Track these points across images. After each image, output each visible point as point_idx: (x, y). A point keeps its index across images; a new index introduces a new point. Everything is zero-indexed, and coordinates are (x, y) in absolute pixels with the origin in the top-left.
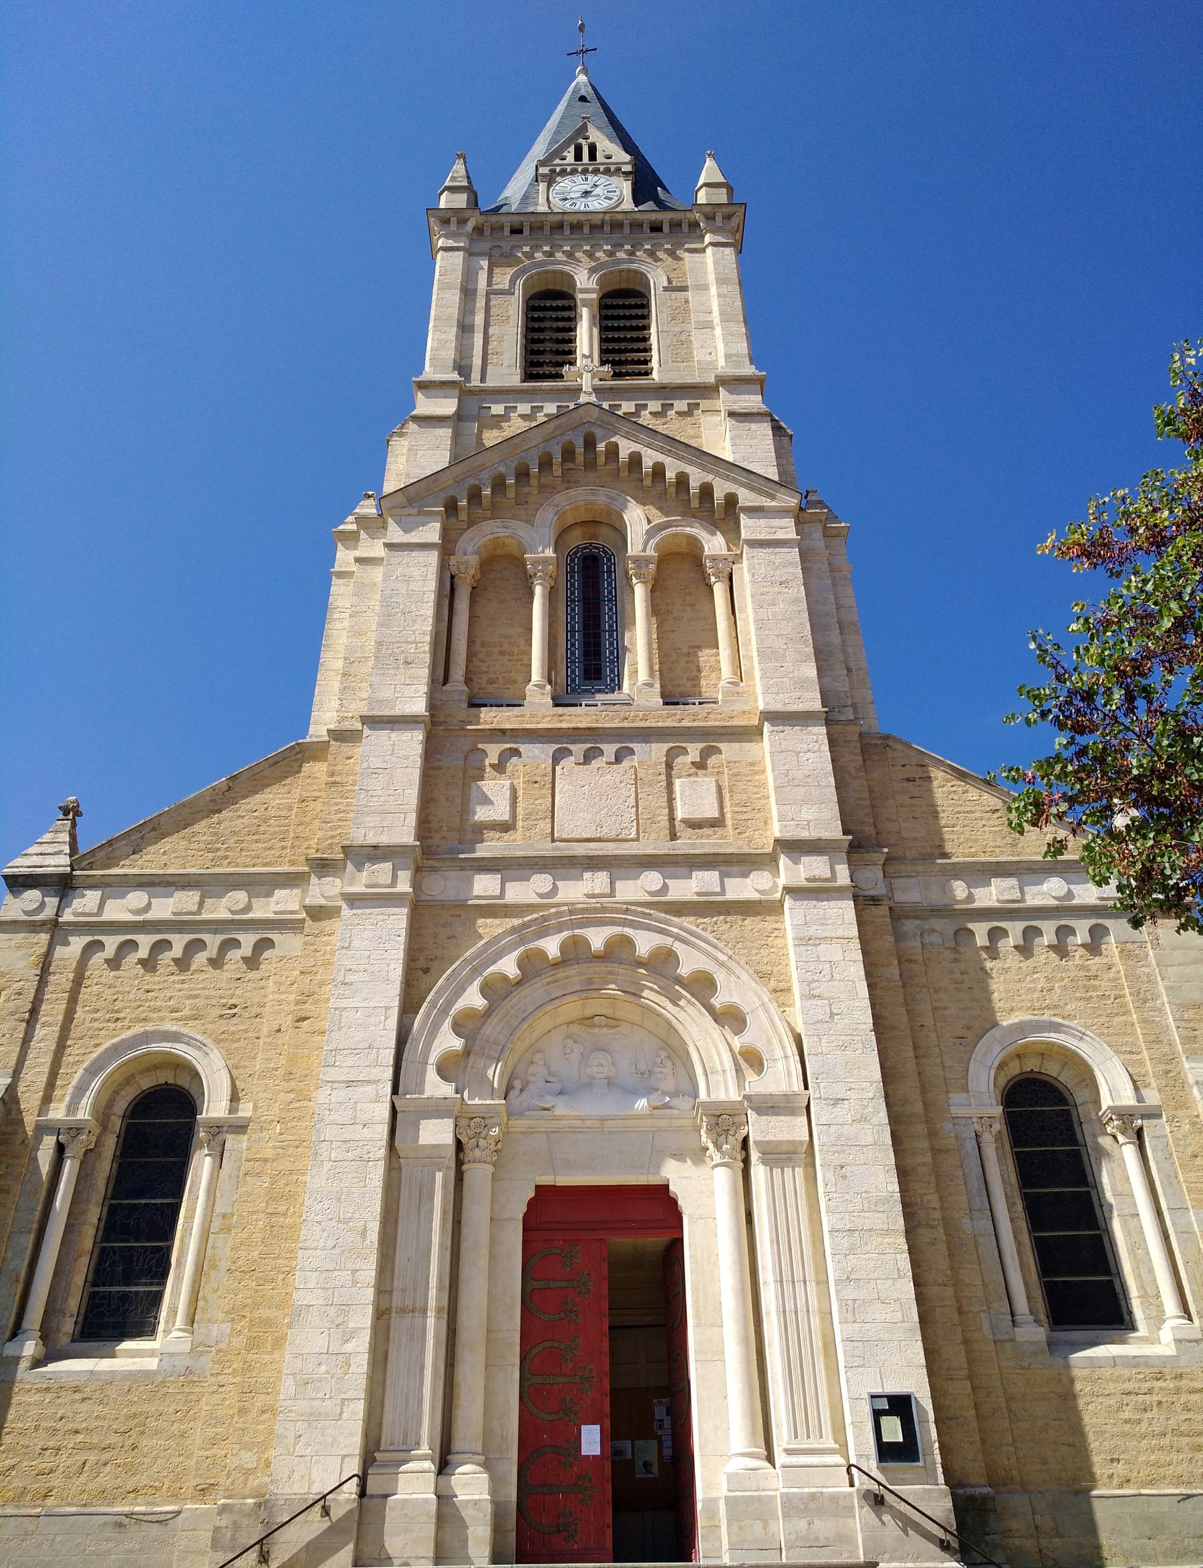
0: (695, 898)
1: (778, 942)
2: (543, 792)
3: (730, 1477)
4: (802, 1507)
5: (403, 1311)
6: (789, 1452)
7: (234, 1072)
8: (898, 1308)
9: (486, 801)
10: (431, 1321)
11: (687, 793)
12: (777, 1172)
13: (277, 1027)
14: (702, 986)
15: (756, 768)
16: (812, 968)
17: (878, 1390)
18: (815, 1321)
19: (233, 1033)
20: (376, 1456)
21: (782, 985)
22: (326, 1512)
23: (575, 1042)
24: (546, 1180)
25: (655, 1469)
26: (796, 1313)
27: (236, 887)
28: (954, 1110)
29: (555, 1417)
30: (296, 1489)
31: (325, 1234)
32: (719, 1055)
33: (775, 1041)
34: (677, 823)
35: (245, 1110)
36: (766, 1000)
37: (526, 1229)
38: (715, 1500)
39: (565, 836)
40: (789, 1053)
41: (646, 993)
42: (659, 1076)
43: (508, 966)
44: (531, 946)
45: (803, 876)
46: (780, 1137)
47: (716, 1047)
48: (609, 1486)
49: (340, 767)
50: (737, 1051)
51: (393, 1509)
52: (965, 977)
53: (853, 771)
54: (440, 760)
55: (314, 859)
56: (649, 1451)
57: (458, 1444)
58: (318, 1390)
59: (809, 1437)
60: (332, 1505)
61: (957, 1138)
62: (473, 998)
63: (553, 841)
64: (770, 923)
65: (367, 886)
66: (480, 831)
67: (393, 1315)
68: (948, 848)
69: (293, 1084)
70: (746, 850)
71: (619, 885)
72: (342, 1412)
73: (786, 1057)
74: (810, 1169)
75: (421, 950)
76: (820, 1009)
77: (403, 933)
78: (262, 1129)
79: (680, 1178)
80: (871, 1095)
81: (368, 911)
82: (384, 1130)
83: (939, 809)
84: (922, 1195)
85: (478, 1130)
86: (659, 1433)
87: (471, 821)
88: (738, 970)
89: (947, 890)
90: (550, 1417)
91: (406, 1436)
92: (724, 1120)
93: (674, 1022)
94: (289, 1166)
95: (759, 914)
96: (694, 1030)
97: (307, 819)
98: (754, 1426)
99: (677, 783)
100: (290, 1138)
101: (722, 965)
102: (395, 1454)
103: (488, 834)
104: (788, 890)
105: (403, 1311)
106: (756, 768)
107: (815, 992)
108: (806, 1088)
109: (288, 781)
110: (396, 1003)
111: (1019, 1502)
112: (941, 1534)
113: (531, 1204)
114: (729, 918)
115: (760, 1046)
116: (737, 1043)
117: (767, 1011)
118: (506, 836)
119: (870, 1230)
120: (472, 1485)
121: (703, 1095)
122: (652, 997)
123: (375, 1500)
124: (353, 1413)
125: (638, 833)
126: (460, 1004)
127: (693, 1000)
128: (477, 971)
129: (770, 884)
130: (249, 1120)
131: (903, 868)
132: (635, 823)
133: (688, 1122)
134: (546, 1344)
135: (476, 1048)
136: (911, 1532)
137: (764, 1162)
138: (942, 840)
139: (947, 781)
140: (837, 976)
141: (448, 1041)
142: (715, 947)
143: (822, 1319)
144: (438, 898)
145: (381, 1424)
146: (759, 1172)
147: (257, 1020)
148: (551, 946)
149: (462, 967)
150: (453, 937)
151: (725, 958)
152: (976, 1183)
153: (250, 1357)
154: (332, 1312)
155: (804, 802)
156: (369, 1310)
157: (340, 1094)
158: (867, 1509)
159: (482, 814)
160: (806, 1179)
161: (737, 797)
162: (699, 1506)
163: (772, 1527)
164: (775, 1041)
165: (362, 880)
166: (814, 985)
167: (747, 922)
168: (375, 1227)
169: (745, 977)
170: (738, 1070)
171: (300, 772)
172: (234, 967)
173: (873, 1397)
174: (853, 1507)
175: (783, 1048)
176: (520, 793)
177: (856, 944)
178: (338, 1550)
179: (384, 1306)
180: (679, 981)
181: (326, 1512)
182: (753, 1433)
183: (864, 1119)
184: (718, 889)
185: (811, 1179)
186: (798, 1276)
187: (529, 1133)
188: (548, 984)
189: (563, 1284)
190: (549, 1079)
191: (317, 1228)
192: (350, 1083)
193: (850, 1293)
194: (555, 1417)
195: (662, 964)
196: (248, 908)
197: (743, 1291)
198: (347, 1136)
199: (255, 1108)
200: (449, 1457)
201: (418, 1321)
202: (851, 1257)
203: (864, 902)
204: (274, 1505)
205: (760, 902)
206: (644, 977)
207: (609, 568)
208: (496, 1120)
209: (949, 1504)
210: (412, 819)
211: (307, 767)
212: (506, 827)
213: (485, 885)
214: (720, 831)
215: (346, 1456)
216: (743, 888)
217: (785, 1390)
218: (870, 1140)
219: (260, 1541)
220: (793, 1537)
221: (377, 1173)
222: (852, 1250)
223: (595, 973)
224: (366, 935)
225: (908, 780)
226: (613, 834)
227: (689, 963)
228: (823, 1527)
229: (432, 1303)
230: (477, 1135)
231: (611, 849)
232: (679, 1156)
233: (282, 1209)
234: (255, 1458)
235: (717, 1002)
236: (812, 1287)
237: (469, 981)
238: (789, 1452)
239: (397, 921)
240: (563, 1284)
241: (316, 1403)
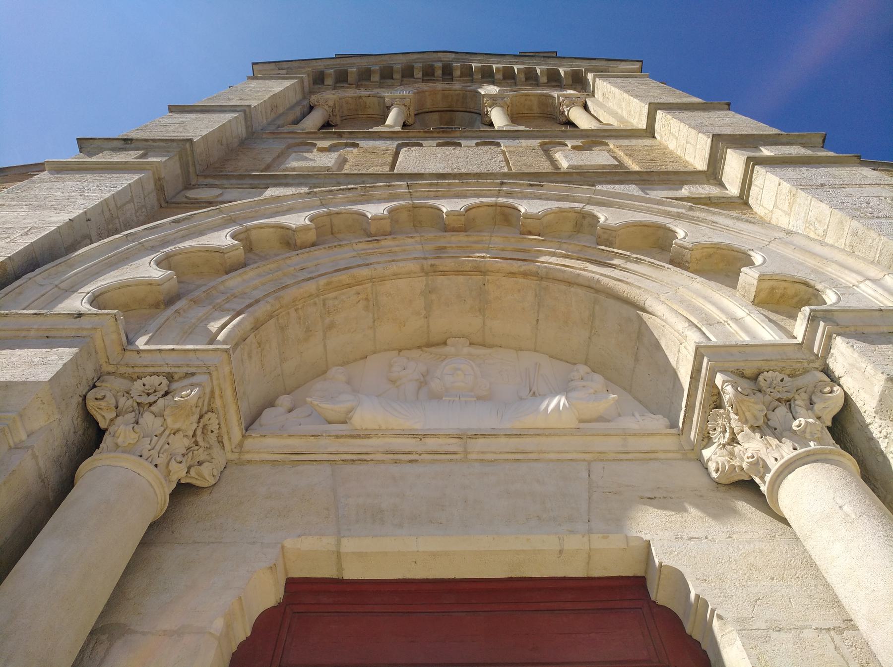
24: (318, 553)
113: (267, 623)
232: (666, 499)
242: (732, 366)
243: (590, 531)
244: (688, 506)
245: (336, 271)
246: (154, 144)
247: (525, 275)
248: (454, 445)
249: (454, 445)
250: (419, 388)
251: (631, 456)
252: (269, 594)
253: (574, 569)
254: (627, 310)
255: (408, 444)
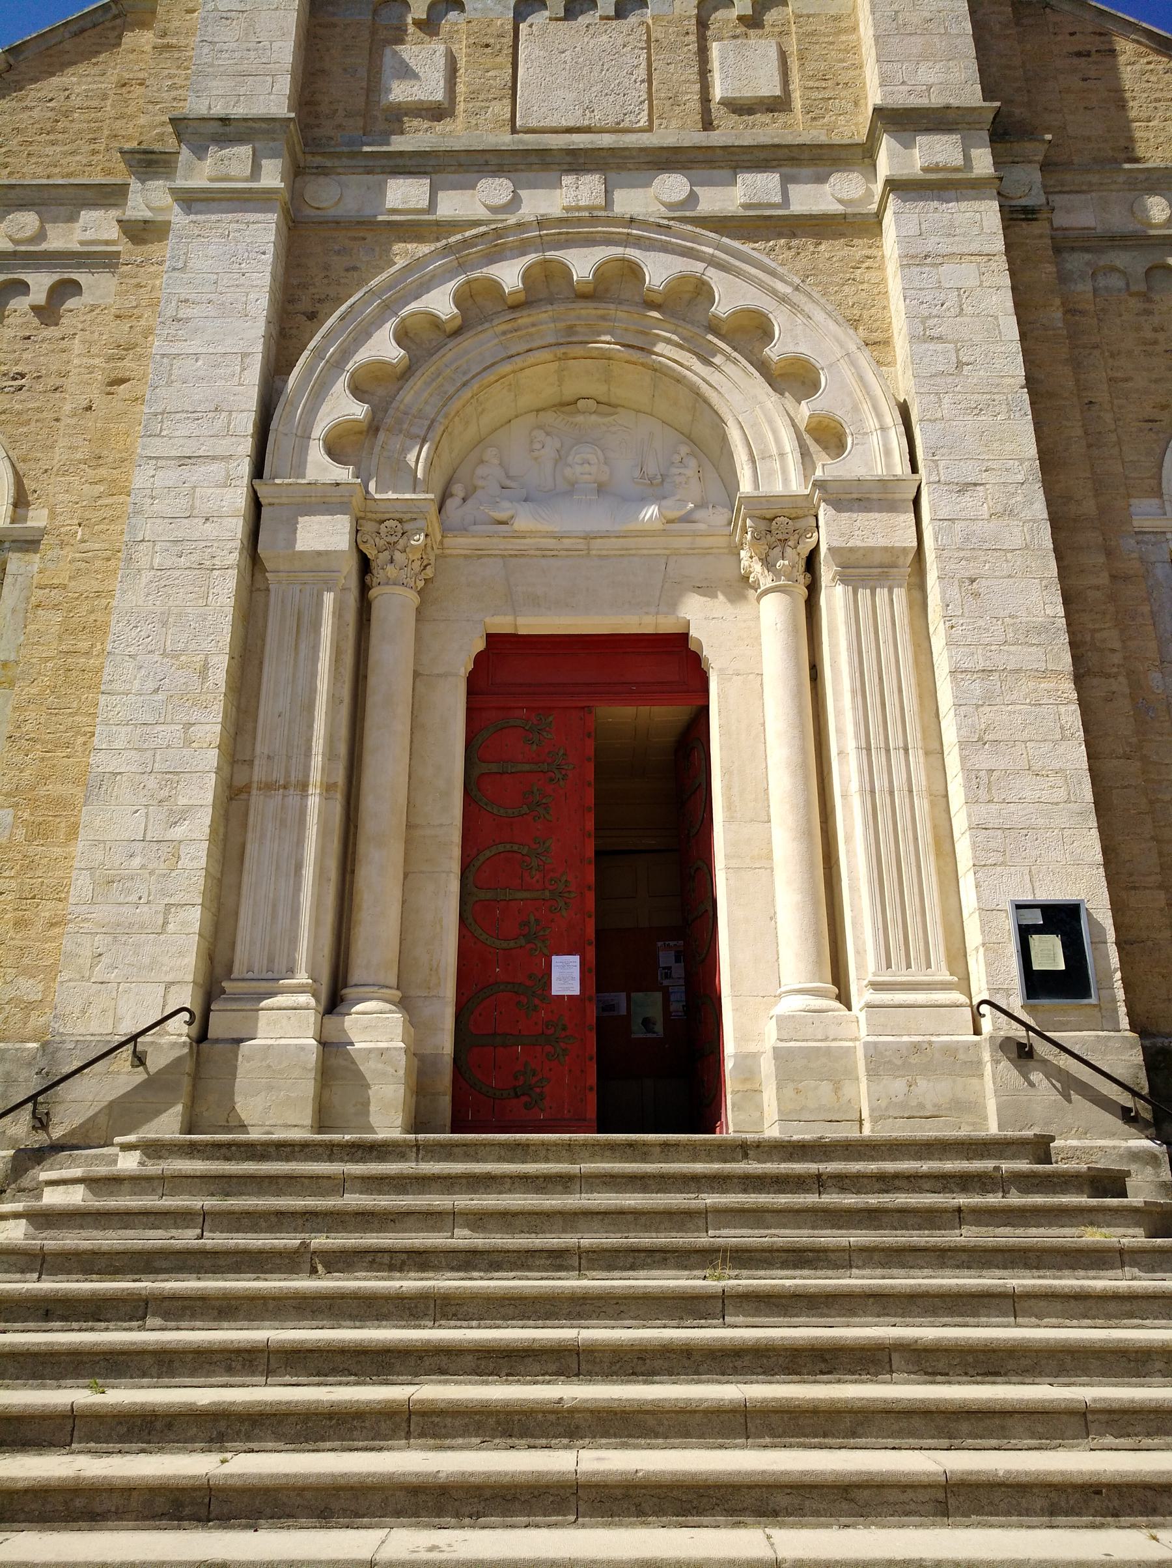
0: (741, 212)
1: (873, 276)
2: (499, 59)
3: (782, 1021)
4: (899, 1062)
5: (269, 787)
6: (877, 986)
7: (20, 466)
8: (1060, 782)
9: (407, 73)
10: (314, 801)
11: (731, 60)
12: (864, 594)
13: (85, 403)
14: (750, 333)
15: (843, 25)
16: (928, 298)
17: (1027, 897)
18: (922, 806)
19: (19, 413)
20: (222, 983)
21: (876, 336)
22: (139, 1059)
23: (548, 434)
24: (503, 624)
25: (659, 1028)
26: (892, 793)
27: (22, 206)
28: (1138, 522)
29: (512, 944)
30: (94, 1027)
31: (143, 671)
32: (775, 432)
33: (866, 408)
34: (714, 106)
35: (37, 518)
36: (852, 347)
37: (471, 692)
38: (755, 1056)
39: (533, 123)
40: (888, 420)
41: (660, 348)
42: (678, 479)
43: (441, 302)
44: (476, 274)
45: (918, 164)
46: (871, 542)
47: (770, 422)
48: (593, 1037)
49: (177, 24)
50: (802, 427)
51: (249, 1059)
52: (1161, 336)
53: (997, 28)
54: (334, 14)
55: (132, 152)
56: (651, 1005)
57: (357, 974)
58: (129, 892)
59: (909, 966)
60: (149, 1050)
61: (1141, 560)
62: (383, 347)
63: (514, 131)
64: (859, 248)
65: (211, 180)
66: (397, 117)
67: (254, 792)
68: (1141, 150)
69: (103, 472)
70: (823, 139)
71: (619, 195)
72: (165, 923)
73: (883, 429)
74: (917, 594)
75: (304, 286)
76: (940, 357)
77: (271, 247)
78: (62, 545)
79: (704, 620)
80: (1020, 478)
81: (214, 217)
82: (237, 527)
83: (1128, 95)
84: (1095, 631)
85: (393, 539)
86: (666, 983)
87: (383, 102)
88: (808, 307)
89: (1134, 209)
90: (504, 945)
91: (271, 960)
92: (777, 523)
93: (704, 387)
94: (96, 585)
95: (842, 235)
96: (735, 398)
97: (129, 111)
98: (819, 954)
99: (715, 50)
100: (97, 546)
101: (783, 300)
102: (254, 984)
103: (411, 123)
104: (894, 185)
105: (269, 787)
106: (843, 25)
107: (935, 333)
108: (915, 469)
109: (102, 57)
110: (258, 348)
112: (1126, 1100)
113: (480, 659)
114: (794, 242)
115: (841, 414)
116: (804, 411)
117: (853, 363)
118: (439, 127)
119: (1017, 671)
120: (376, 1029)
121: (746, 487)
122: (667, 352)
123: (219, 1047)
124: (183, 924)
125: (650, 120)
126: (363, 355)
127: (735, 354)
128: (388, 309)
129: (861, 192)
130: (43, 531)
131: (1068, 177)
132: (646, 106)
133: (722, 541)
134: (501, 848)
135: (389, 421)
136: (1075, 1097)
137: (844, 579)
138: (1131, 139)
139: (1140, 55)
140: (968, 310)
141: (343, 407)
142: (773, 273)
143: (933, 805)
144: (332, 212)
145: (233, 945)
146: (834, 598)
147: (57, 395)
148: (509, 275)
149: (365, 302)
150: (355, 269)
151: (788, 290)
153: (31, 850)
154: (152, 782)
155: (923, 57)
156: (211, 780)
157: (170, 476)
158: (1005, 1064)
159: (400, 92)
160: (911, 606)
161: (811, 67)
162: (729, 1064)
163: (848, 1090)
164: (866, 408)
165: (200, 172)
166: (930, 322)
167: (822, 247)
168: (220, 664)
169: (819, 316)
170: (805, 454)
171: (119, 45)
172: (20, 320)
173: (1019, 907)
174: (980, 1063)
175: (879, 415)
176: (462, 63)
177: (1002, 263)
178: (158, 1113)
179: (240, 781)
180: (713, 327)
181: (139, 1059)
182: (818, 962)
183: (1008, 512)
184: (778, 199)
185: (919, 605)
186: (895, 741)
187: (478, 555)
188: (504, 333)
189: (527, 767)
190: (508, 483)
191: (130, 665)
192: (184, 460)
193: (984, 760)
194: (512, 944)
195: (687, 303)
196: (41, 236)
197: (804, 765)
198: (180, 535)
199: (53, 515)
200: (344, 992)
201: (293, 799)
202: (987, 709)
203: (1015, 216)
204: (57, 1050)
205: (845, 216)
206: (658, 323)
208: (420, 523)
209: (1137, 1057)
210: (284, 85)
211: (129, 38)
212: (438, 112)
213: (404, 194)
214: (782, 118)
215: (173, 983)
216: (814, 198)
217: (873, 904)
218: (1018, 542)
219: (33, 1098)
220: (883, 1103)
221: (225, 590)
222: (988, 699)
223: (579, 318)
224: (212, 250)
225: (1079, 54)
226: (611, 121)
227: (729, 296)
228: (931, 1090)
229: (316, 776)
230: (391, 546)
232: (706, 589)
233: (84, 645)
234: (41, 987)
235: (773, 352)
236: (917, 758)
237: (377, 322)
238: (877, 986)
239: (261, 234)
240: (527, 767)
241: (124, 909)
242: (758, 513)
243: (657, 613)
244: (719, 594)
245: (485, 369)
246: (254, 125)
247: (642, 364)
248: (581, 544)
249: (581, 544)
250: (556, 465)
251: (696, 551)
252: (480, 645)
253: (649, 630)
254: (718, 420)
255: (550, 543)
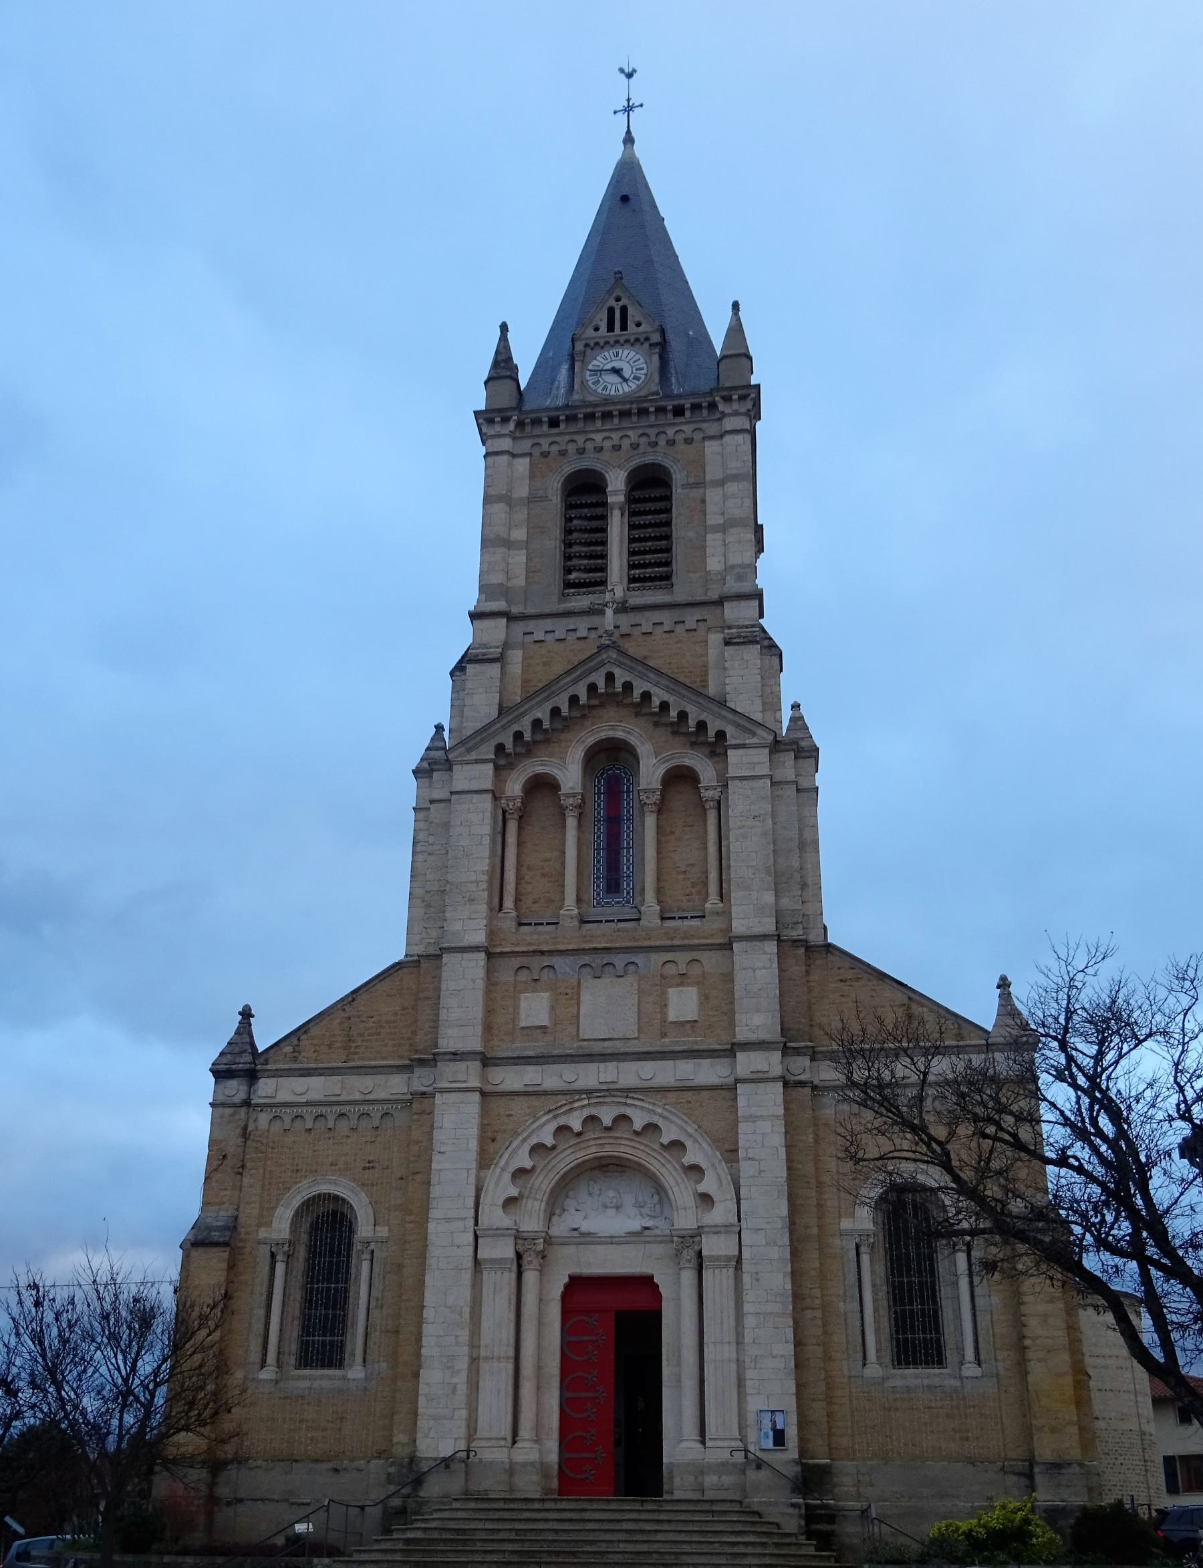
5: (486, 1358)
107: (750, 1156)
108: (739, 1221)
111: (848, 1465)
145: (476, 1421)
152: (852, 1278)
156: (466, 1359)
179: (475, 1356)
207: (628, 788)
231: (620, 1047)
252: (566, 1280)
